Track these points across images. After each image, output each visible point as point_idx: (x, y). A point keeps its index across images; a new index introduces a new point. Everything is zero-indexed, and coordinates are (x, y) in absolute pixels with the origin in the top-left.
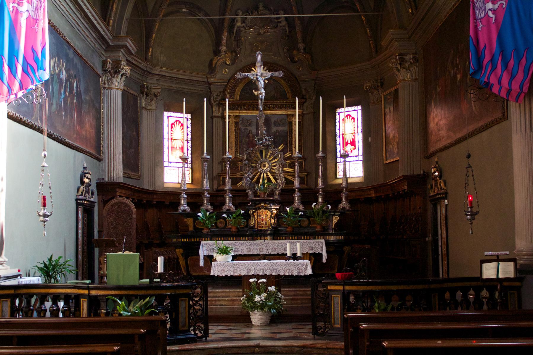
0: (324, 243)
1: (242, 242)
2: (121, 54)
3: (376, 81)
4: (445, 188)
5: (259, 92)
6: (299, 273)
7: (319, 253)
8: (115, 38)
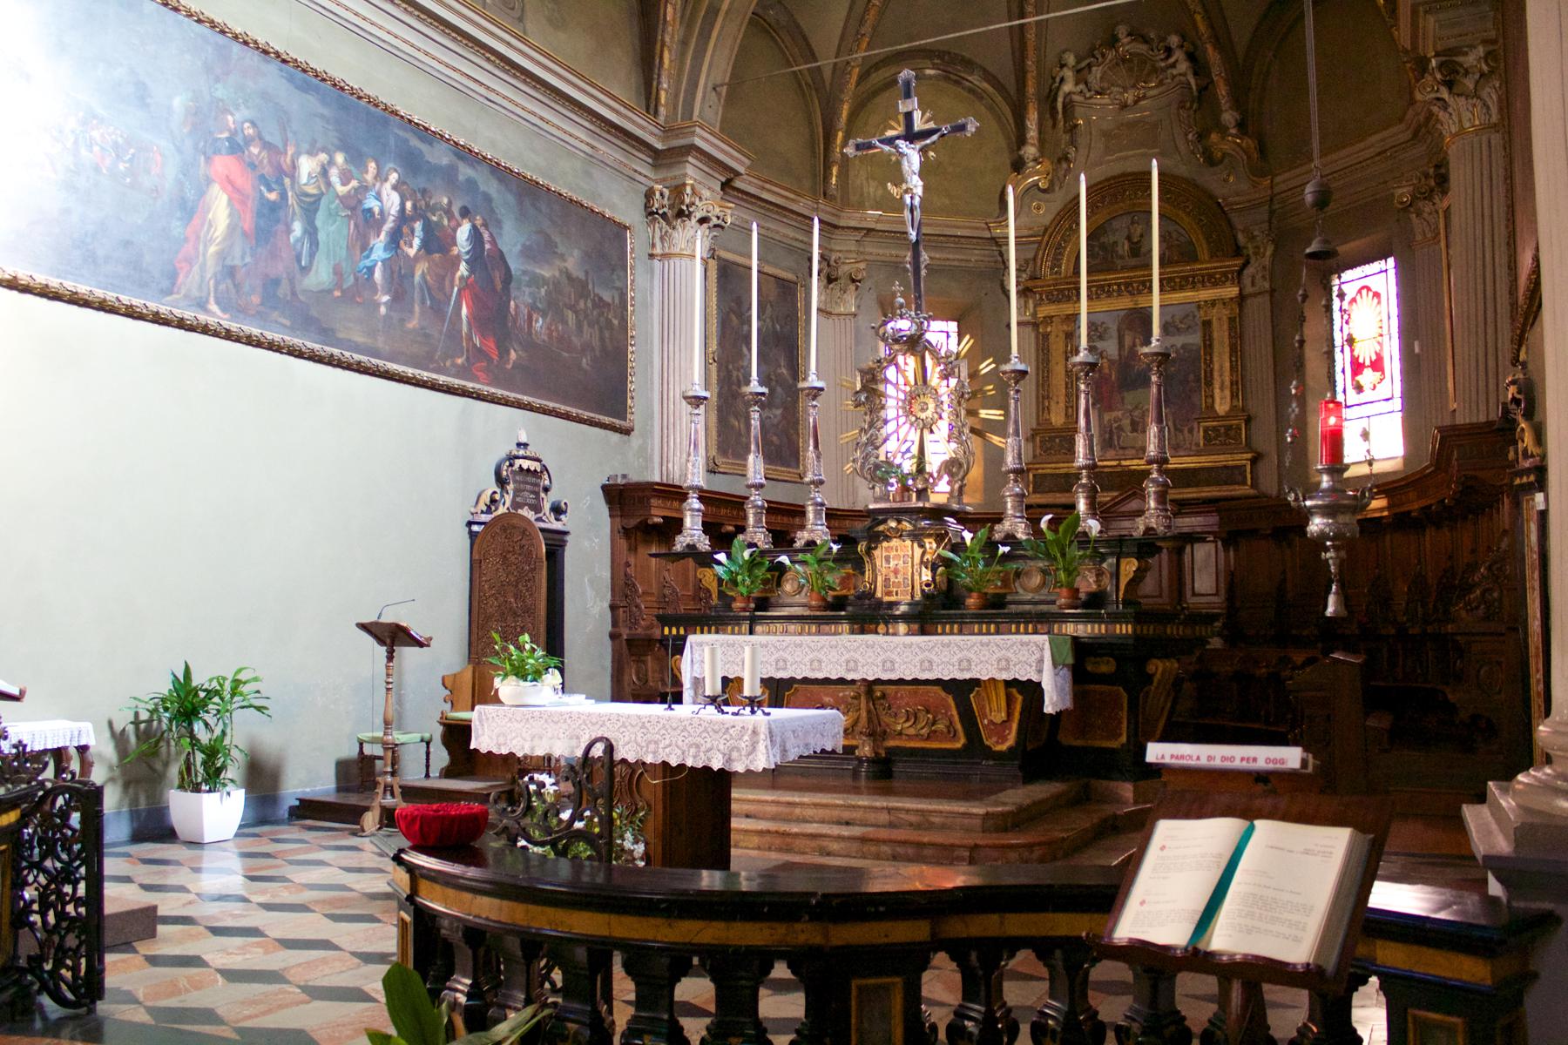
0: (1047, 646)
1: (946, 638)
2: (692, 172)
3: (1427, 176)
4: (1536, 451)
5: (904, 186)
6: (729, 760)
7: (1030, 681)
8: (668, 131)
